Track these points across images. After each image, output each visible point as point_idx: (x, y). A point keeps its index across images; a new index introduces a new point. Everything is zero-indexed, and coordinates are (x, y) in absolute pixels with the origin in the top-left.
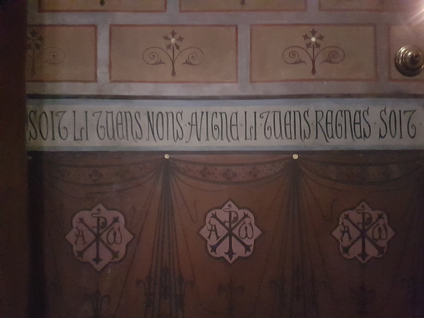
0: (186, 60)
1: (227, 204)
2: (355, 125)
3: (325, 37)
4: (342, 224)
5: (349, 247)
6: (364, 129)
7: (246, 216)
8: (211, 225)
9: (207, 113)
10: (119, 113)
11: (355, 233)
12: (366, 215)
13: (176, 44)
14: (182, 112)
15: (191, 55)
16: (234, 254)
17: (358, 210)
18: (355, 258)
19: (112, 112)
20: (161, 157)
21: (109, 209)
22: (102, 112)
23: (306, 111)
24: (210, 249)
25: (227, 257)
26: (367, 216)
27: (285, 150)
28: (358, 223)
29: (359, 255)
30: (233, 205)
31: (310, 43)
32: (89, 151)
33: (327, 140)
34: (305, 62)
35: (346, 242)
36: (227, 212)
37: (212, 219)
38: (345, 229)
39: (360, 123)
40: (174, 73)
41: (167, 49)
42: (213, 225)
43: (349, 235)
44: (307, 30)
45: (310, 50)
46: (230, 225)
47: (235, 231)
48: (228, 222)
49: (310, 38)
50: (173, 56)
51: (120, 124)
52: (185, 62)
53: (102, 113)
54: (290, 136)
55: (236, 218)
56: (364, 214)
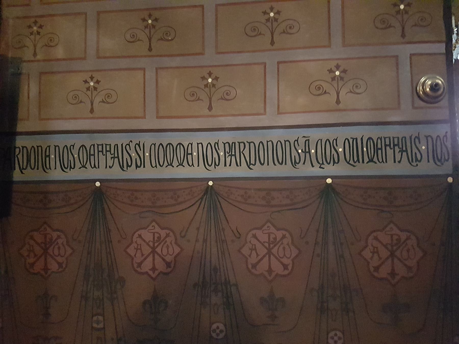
0: (222, 97)
1: (266, 226)
2: (118, 156)
3: (220, 78)
4: (136, 242)
5: (142, 262)
6: (215, 158)
7: (59, 237)
8: (252, 244)
10: (190, 144)
12: (394, 236)
19: (110, 145)
21: (278, 230)
24: (135, 265)
26: (272, 236)
29: (150, 270)
31: (89, 87)
33: (45, 171)
36: (151, 232)
37: (138, 239)
38: (138, 247)
39: (407, 151)
40: (210, 108)
41: (87, 91)
42: (375, 247)
44: (86, 76)
47: (158, 250)
48: (266, 242)
50: (210, 94)
53: (23, 146)
54: (155, 165)
55: (159, 238)
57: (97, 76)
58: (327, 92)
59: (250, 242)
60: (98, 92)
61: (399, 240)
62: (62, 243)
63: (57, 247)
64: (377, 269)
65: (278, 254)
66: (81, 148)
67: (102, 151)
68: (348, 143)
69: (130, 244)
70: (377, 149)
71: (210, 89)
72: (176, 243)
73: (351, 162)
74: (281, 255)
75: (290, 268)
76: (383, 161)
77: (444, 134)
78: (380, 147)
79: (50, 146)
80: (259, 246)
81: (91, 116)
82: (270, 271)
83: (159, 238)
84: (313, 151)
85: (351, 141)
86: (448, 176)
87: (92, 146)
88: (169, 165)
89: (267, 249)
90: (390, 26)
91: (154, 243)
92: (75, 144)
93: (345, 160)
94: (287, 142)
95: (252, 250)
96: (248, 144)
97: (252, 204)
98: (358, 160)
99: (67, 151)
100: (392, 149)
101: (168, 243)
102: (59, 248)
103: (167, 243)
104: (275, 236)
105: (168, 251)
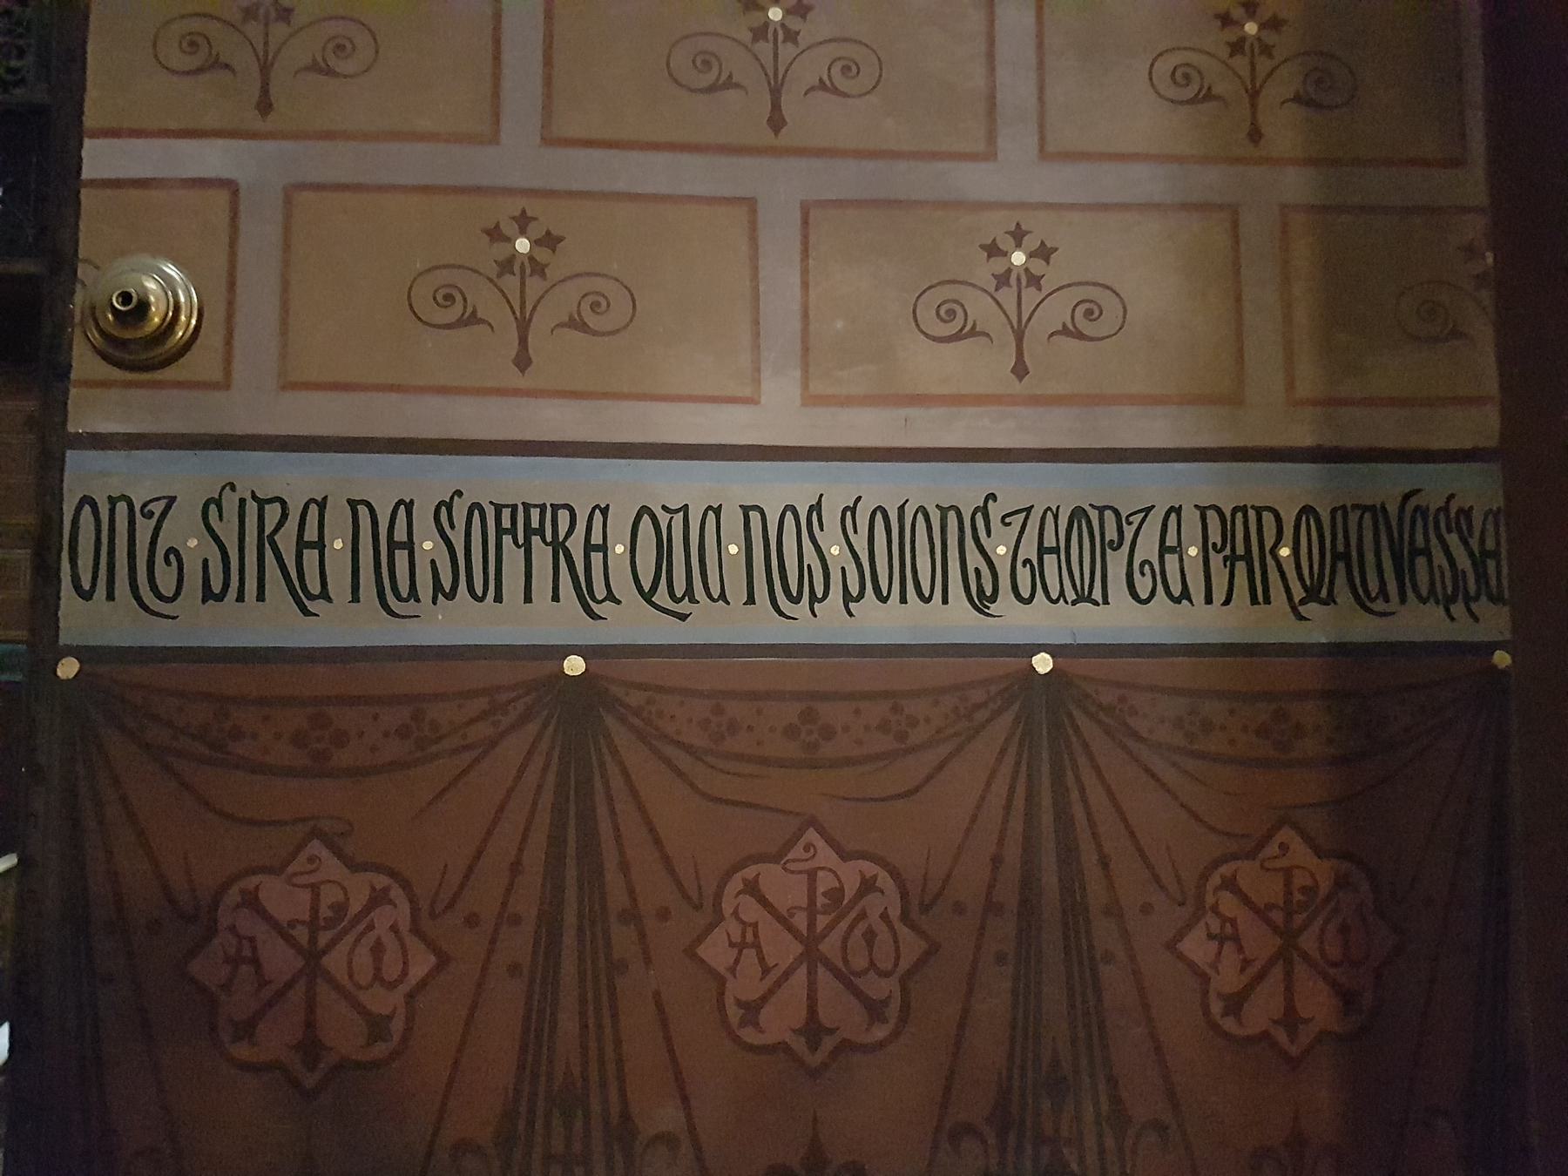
1: (302, 857)
7: (378, 899)
8: (743, 923)
10: (710, 512)
13: (1027, 270)
14: (325, 498)
15: (443, 289)
17: (295, 874)
18: (1265, 1035)
19: (685, 508)
20: (549, 667)
22: (349, 501)
24: (734, 1014)
25: (1281, 1036)
32: (196, 645)
34: (988, 335)
35: (746, 985)
36: (800, 872)
40: (523, 362)
46: (811, 924)
52: (1061, 328)
57: (1040, 228)
58: (977, 330)
59: (735, 913)
60: (1044, 293)
64: (1235, 1004)
67: (513, 531)
70: (1410, 552)
71: (523, 284)
72: (416, 930)
73: (662, 597)
76: (1062, 593)
77: (1441, 503)
79: (687, 505)
80: (769, 930)
81: (1017, 387)
82: (813, 1030)
84: (619, 549)
85: (663, 518)
86: (1494, 646)
89: (1275, 929)
90: (730, 84)
91: (1289, 915)
93: (1000, 592)
94: (1265, 514)
95: (234, 961)
96: (1097, 512)
97: (740, 757)
98: (689, 591)
99: (92, 519)
100: (172, 550)
101: (382, 930)
103: (376, 932)
105: (378, 969)
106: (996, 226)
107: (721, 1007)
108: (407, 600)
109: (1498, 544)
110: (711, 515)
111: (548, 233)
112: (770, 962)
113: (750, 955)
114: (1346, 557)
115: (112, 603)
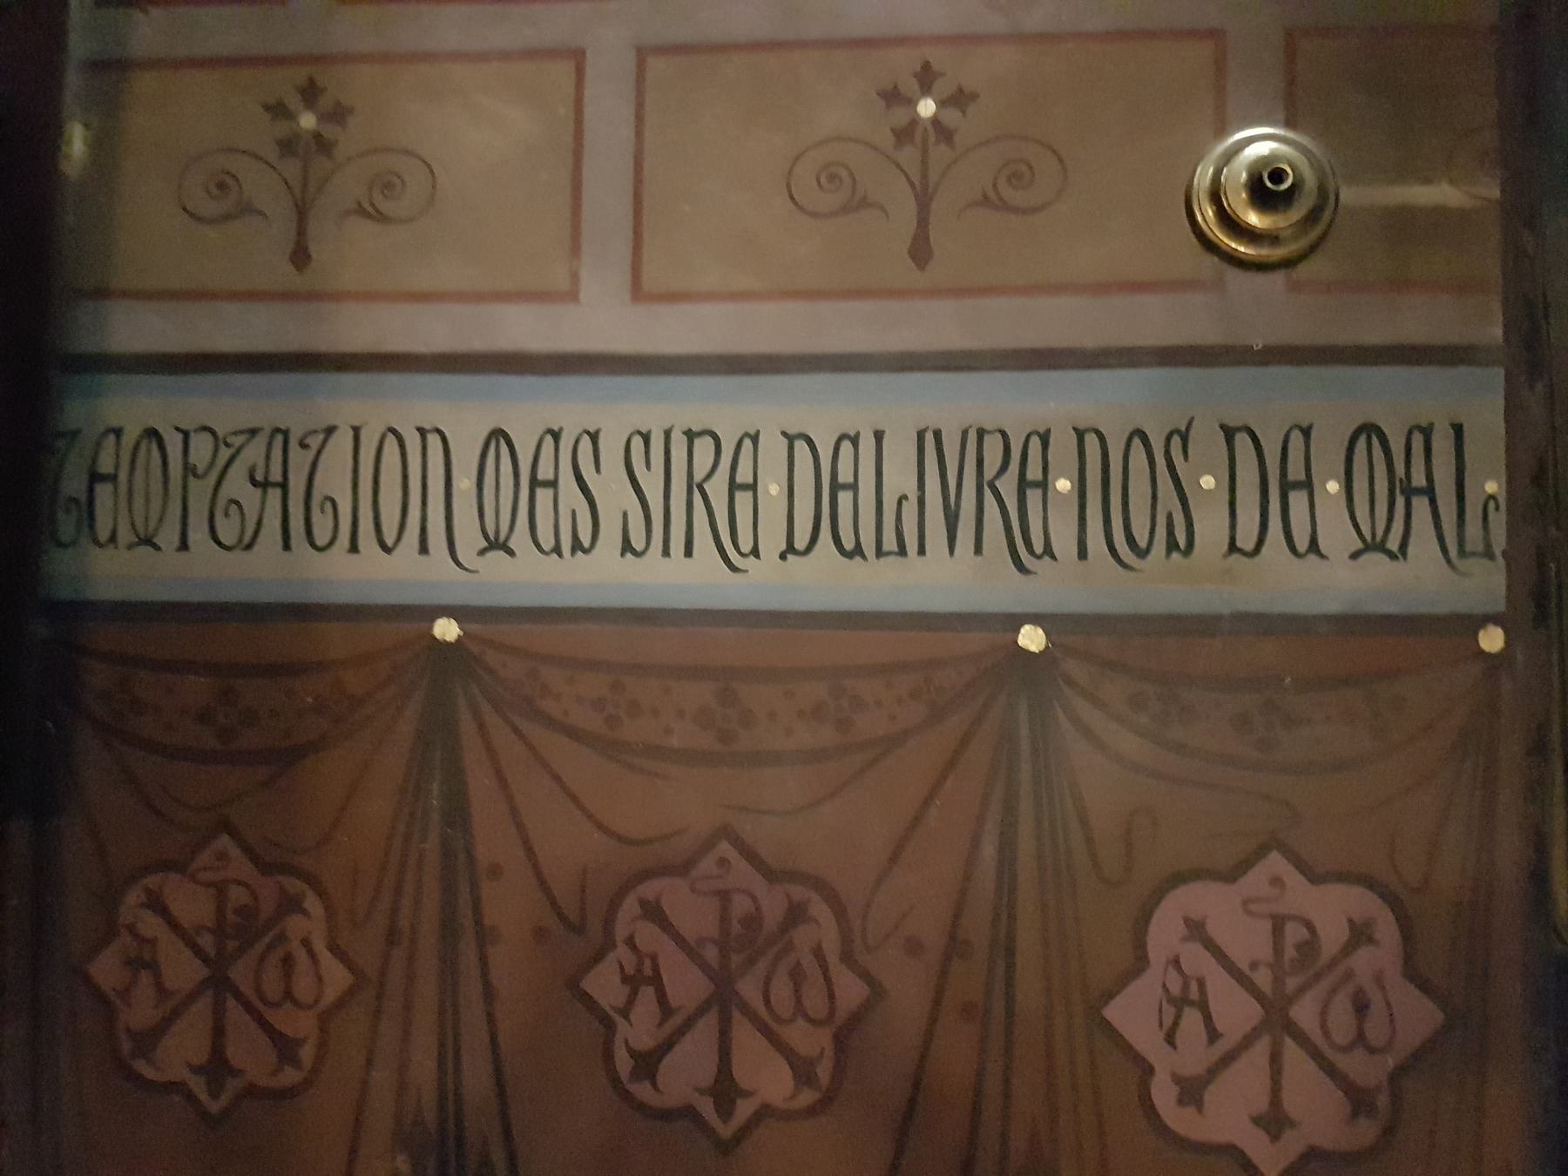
4: (630, 942)
9: (879, 436)
11: (182, 970)
16: (746, 1094)
23: (1178, 431)
24: (623, 1063)
27: (741, 608)
28: (1254, 965)
29: (196, 1070)
30: (235, 852)
35: (640, 1030)
40: (920, 252)
43: (1208, 1019)
44: (903, 63)
45: (909, 155)
46: (1278, 981)
49: (912, 103)
51: (1036, 484)
54: (751, 544)
55: (1309, 948)
56: (724, 896)
61: (753, 921)
62: (306, 943)
63: (274, 959)
65: (767, 1002)
66: (1362, 442)
68: (982, 450)
69: (599, 957)
74: (273, 988)
75: (307, 1053)
78: (1302, 477)
82: (217, 1067)
83: (1309, 948)
84: (774, 489)
87: (586, 439)
88: (1368, 547)
89: (206, 960)
92: (1195, 423)
94: (194, 440)
102: (288, 961)
104: (753, 910)
105: (799, 1001)
106: (903, 63)
107: (608, 1056)
108: (1039, 557)
109: (117, 467)
110: (747, 443)
111: (961, 90)
112: (1220, 1026)
113: (647, 993)
114: (1286, 487)
115: (667, 559)
